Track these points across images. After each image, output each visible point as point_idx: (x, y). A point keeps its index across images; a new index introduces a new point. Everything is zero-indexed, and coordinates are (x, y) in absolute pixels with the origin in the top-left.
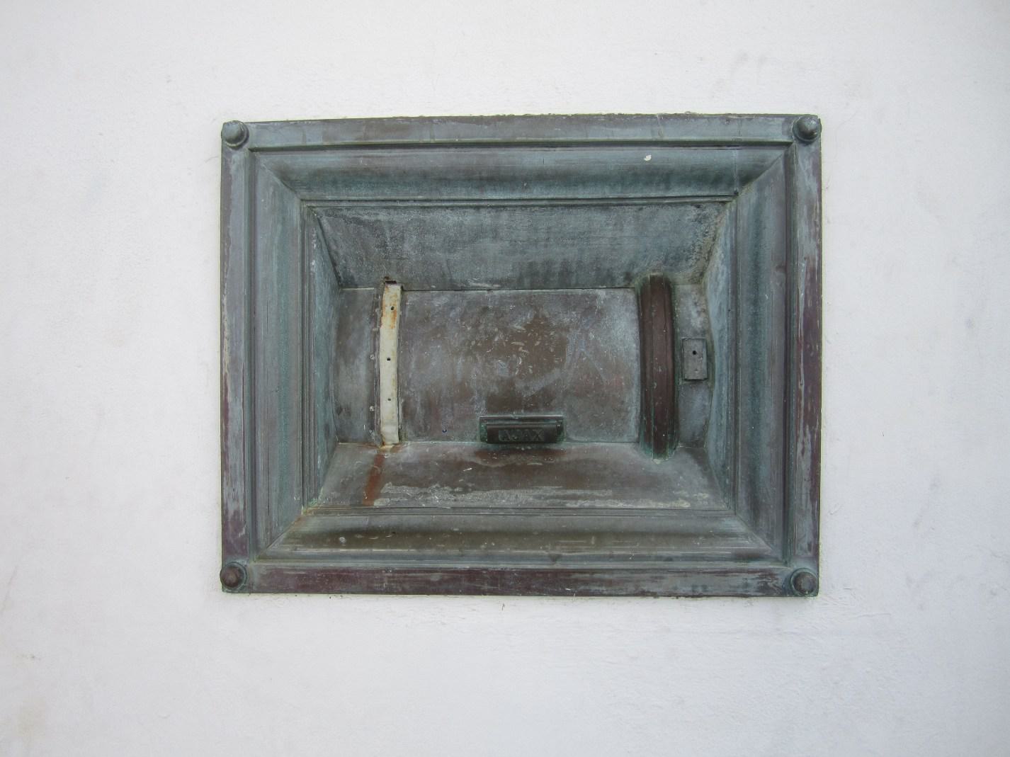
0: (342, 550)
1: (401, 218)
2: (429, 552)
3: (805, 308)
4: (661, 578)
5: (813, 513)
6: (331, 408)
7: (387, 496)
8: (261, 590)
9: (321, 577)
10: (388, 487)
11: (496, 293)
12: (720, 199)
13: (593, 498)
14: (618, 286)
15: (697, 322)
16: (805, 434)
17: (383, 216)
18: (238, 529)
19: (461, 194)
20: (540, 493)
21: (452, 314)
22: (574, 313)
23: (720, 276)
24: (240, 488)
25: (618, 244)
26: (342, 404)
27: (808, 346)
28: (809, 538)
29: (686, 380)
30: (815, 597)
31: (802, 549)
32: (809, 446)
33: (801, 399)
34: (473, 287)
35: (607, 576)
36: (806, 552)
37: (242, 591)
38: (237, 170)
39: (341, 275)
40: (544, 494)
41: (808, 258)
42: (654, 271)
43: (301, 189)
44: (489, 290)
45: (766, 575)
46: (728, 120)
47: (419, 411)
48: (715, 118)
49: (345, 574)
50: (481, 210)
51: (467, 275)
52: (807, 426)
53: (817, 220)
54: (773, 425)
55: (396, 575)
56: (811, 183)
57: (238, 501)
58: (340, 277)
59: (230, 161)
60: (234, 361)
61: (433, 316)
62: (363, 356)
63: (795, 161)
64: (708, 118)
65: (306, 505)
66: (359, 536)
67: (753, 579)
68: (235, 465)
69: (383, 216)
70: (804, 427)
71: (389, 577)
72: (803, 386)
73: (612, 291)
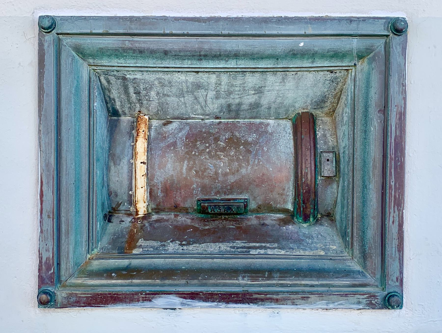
0: (114, 281)
1: (150, 77)
2: (167, 282)
3: (395, 136)
4: (308, 297)
5: (399, 259)
6: (105, 191)
7: (140, 246)
8: (63, 306)
9: (101, 297)
10: (141, 242)
11: (207, 121)
12: (345, 68)
13: (265, 248)
14: (282, 118)
15: (331, 141)
16: (394, 212)
17: (138, 76)
18: (48, 269)
19: (187, 63)
20: (234, 245)
21: (180, 135)
22: (255, 135)
23: (344, 114)
24: (51, 244)
25: (282, 94)
26: (112, 190)
27: (397, 159)
28: (397, 274)
29: (322, 177)
30: (401, 308)
31: (392, 280)
32: (397, 219)
33: (392, 190)
34: (193, 118)
35: (275, 297)
36: (395, 282)
37: (52, 307)
38: (48, 47)
39: (111, 109)
40: (236, 245)
41: (398, 106)
42: (304, 109)
43: (88, 58)
44: (202, 120)
45: (371, 296)
46: (351, 21)
47: (160, 194)
48: (343, 19)
49: (116, 296)
50: (199, 73)
51: (189, 111)
52: (396, 207)
53: (404, 83)
54: (375, 207)
55: (147, 296)
56: (400, 59)
57: (49, 251)
58: (110, 111)
59: (44, 41)
60: (48, 165)
61: (168, 136)
62: (125, 161)
63: (391, 46)
64: (339, 20)
65: (90, 253)
66: (124, 273)
67: (363, 299)
68: (47, 229)
69: (138, 76)
70: (394, 207)
71: (143, 298)
72: (394, 182)
73: (277, 120)
